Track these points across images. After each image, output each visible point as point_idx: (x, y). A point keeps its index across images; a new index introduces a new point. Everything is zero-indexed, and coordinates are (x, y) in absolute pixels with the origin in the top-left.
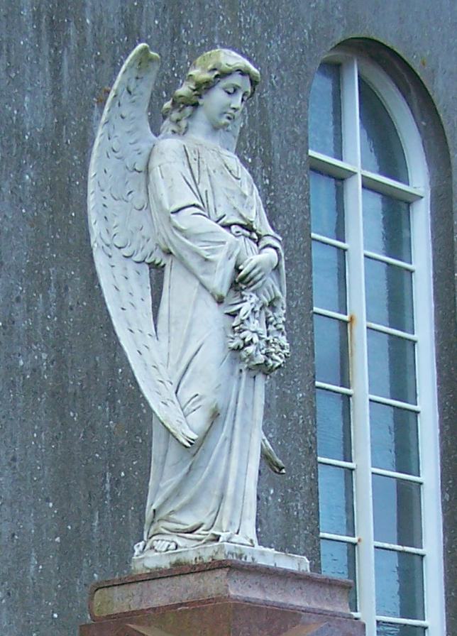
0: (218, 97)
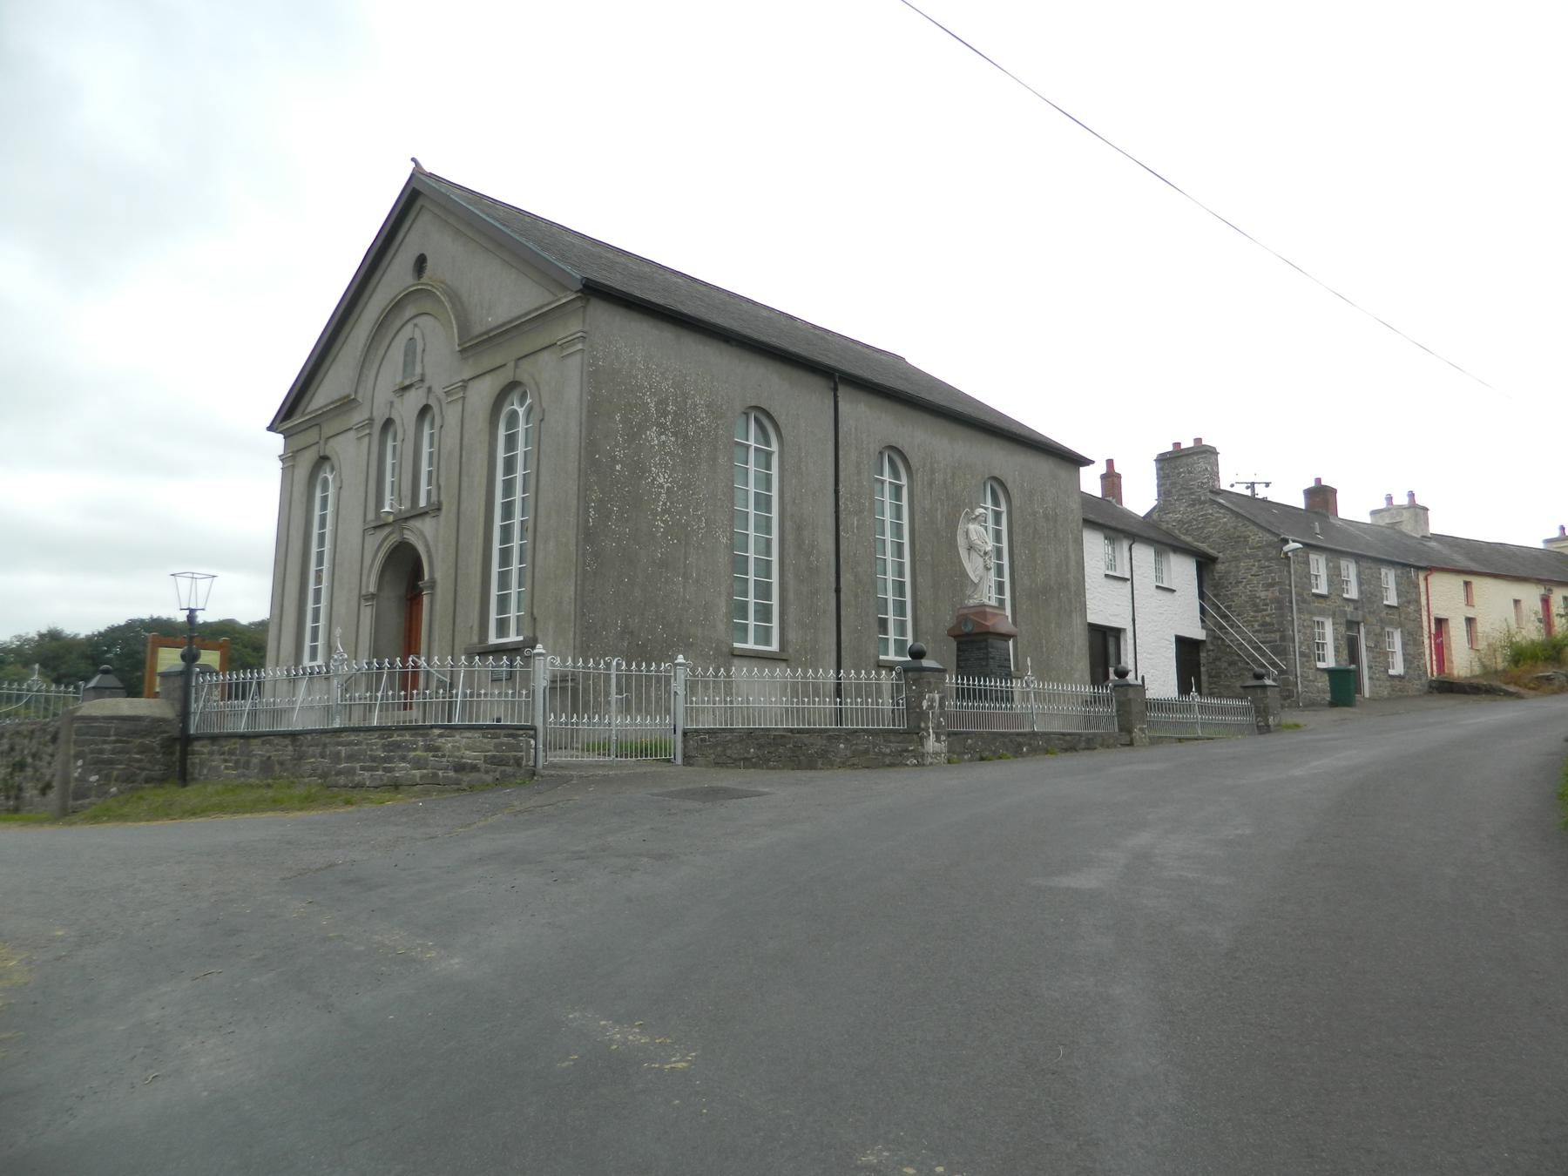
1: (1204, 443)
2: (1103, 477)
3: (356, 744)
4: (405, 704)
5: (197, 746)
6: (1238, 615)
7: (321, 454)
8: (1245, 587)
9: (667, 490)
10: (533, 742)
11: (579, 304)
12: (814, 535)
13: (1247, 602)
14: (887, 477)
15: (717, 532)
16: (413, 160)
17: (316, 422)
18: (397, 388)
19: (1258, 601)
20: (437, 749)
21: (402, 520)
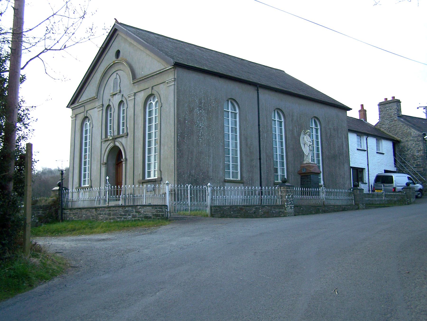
0: (308, 133)
1: (395, 98)
2: (360, 111)
3: (115, 211)
4: (118, 199)
5: (65, 211)
6: (408, 162)
7: (85, 116)
8: (410, 151)
9: (202, 128)
10: (167, 210)
11: (173, 70)
12: (251, 140)
13: (411, 157)
14: (314, 126)
15: (219, 141)
16: (115, 19)
17: (83, 105)
18: (111, 94)
19: (415, 156)
20: (139, 212)
21: (114, 139)
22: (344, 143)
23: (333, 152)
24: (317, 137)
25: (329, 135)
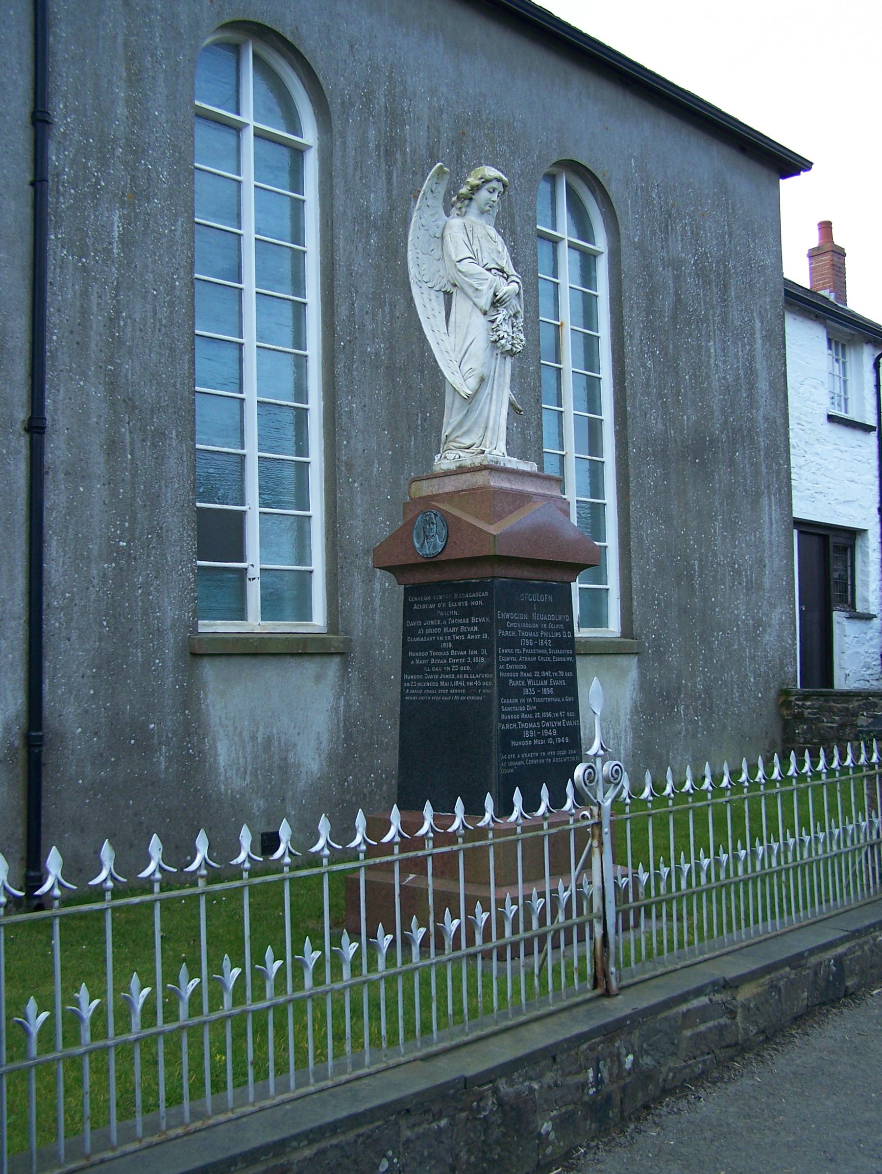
0: (484, 194)
14: (564, 229)
22: (760, 366)
23: (694, 417)
24: (588, 305)
25: (667, 303)
